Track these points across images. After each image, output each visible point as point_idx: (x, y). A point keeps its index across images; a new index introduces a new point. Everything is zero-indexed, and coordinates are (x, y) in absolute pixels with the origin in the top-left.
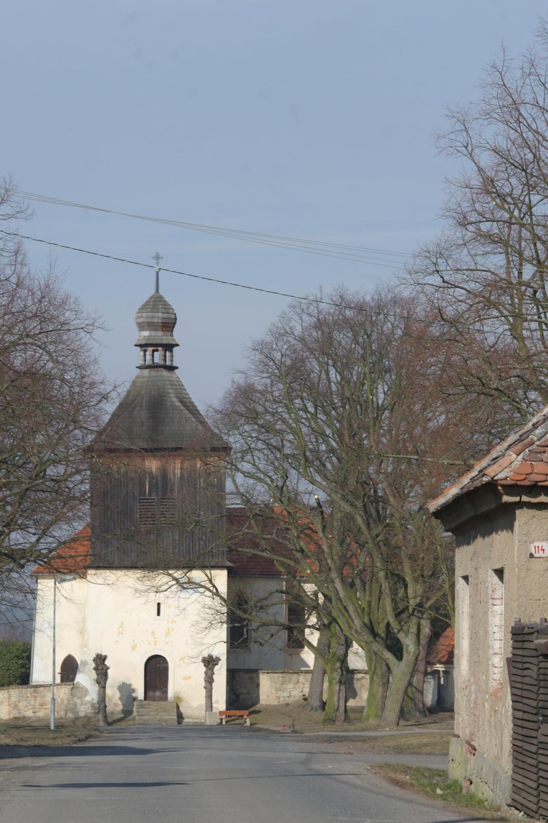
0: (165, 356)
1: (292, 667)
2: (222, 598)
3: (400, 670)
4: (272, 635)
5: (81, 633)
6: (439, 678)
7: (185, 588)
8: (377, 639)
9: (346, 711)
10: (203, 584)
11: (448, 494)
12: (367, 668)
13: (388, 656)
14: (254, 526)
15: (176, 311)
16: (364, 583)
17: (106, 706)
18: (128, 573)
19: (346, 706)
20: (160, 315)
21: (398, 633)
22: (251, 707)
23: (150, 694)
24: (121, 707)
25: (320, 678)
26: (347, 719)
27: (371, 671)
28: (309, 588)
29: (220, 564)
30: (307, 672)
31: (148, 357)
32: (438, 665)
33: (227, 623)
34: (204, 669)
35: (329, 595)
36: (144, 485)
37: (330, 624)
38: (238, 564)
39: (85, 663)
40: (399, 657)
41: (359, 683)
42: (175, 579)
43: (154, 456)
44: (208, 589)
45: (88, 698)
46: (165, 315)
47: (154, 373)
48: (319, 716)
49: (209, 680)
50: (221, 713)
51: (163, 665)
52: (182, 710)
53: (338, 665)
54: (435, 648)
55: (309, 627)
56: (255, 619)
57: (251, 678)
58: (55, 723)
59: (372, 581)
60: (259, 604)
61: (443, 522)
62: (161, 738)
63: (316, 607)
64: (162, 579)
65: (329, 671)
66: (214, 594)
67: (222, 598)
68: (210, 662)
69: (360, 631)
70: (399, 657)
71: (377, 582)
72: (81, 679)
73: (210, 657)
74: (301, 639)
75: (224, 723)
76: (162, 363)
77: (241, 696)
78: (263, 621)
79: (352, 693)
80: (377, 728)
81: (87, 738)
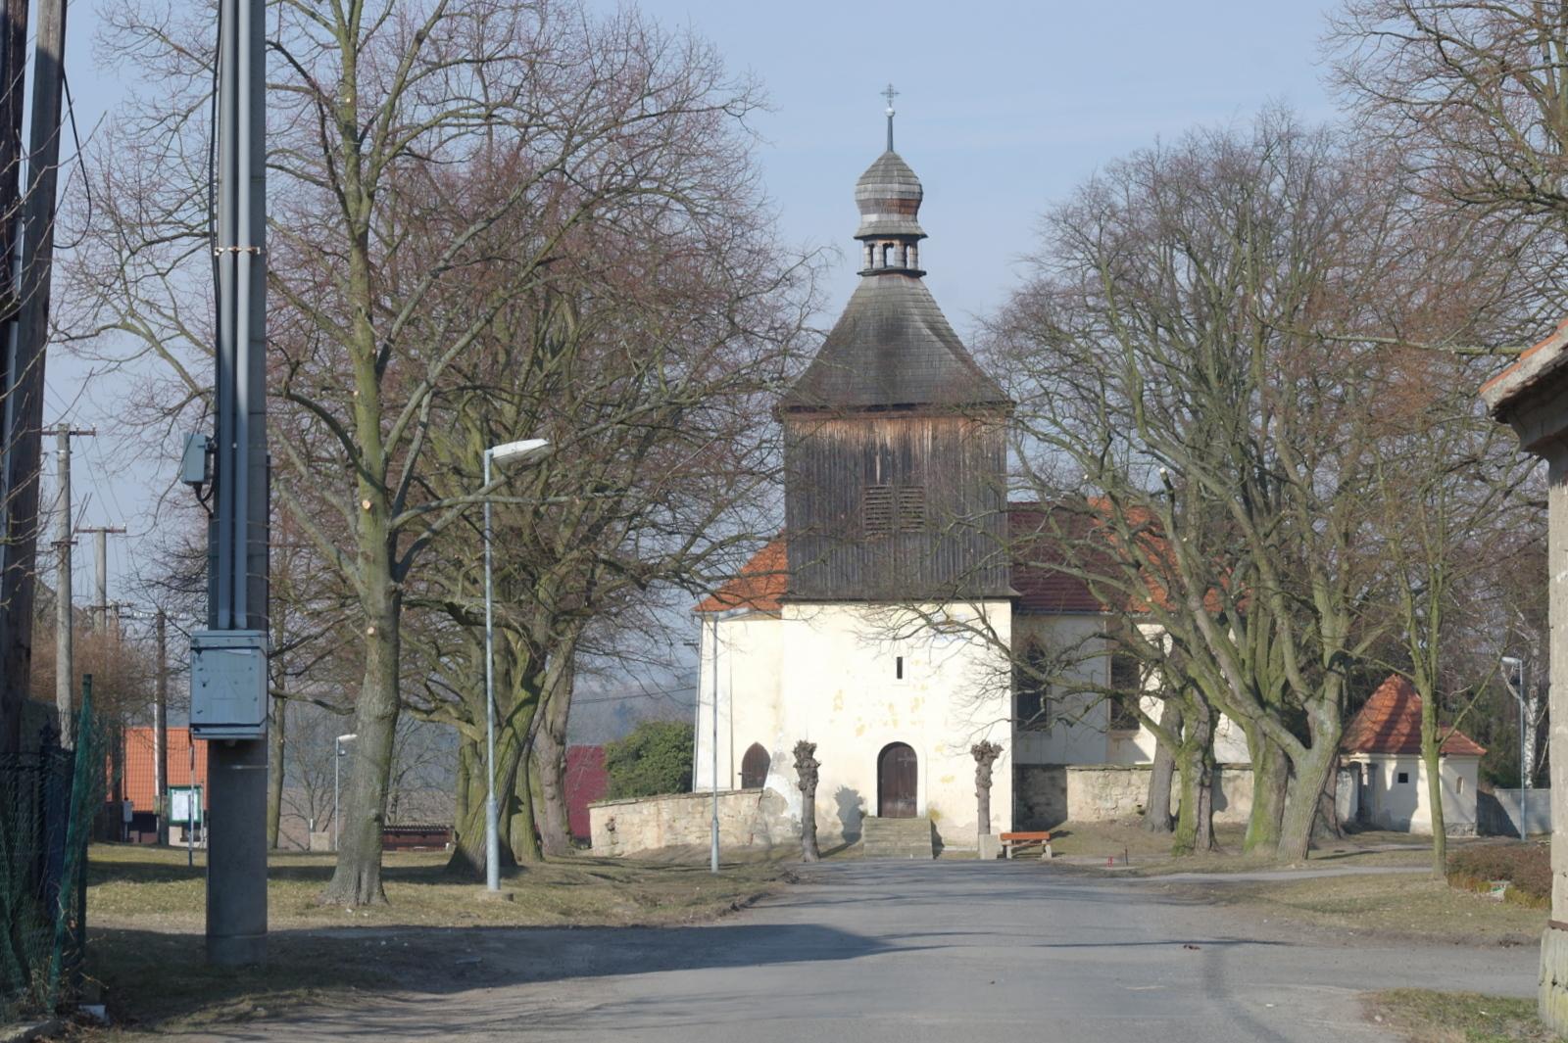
0: (905, 254)
1: (1117, 759)
2: (1002, 647)
3: (1310, 763)
4: (1088, 709)
5: (774, 707)
6: (1361, 776)
7: (942, 632)
8: (1268, 710)
9: (1212, 833)
10: (970, 624)
11: (1530, 363)
12: (1249, 761)
13: (1290, 740)
14: (1055, 527)
15: (921, 181)
16: (1243, 620)
17: (815, 827)
18: (846, 608)
19: (1211, 825)
20: (896, 186)
21: (1306, 700)
22: (1053, 826)
23: (888, 805)
24: (841, 828)
25: (1166, 778)
26: (1213, 845)
27: (1259, 766)
28: (1147, 630)
29: (1000, 593)
30: (1143, 768)
31: (877, 257)
32: (1358, 755)
33: (1011, 687)
34: (976, 765)
35: (1185, 638)
36: (874, 462)
37: (1183, 689)
38: (1029, 591)
39: (781, 757)
40: (1307, 742)
41: (1231, 784)
42: (923, 616)
43: (890, 419)
44: (980, 633)
45: (786, 814)
46: (904, 188)
47: (886, 282)
48: (1168, 840)
49: (984, 783)
50: (1004, 836)
51: (908, 759)
52: (941, 832)
53: (1198, 756)
54: (1354, 726)
55: (1149, 694)
56: (1059, 682)
57: (1053, 778)
58: (719, 858)
59: (1257, 615)
60: (1064, 657)
61: (1522, 430)
62: (897, 899)
63: (1159, 661)
64: (900, 615)
65: (1183, 767)
66: (989, 641)
67: (1002, 647)
68: (985, 754)
69: (1239, 697)
70: (1307, 742)
71: (1266, 615)
72: (774, 782)
73: (986, 745)
74: (1135, 714)
75: (1009, 855)
76: (899, 265)
77: (1037, 809)
78: (1072, 685)
79: (1219, 802)
80: (1270, 865)
81: (753, 900)
